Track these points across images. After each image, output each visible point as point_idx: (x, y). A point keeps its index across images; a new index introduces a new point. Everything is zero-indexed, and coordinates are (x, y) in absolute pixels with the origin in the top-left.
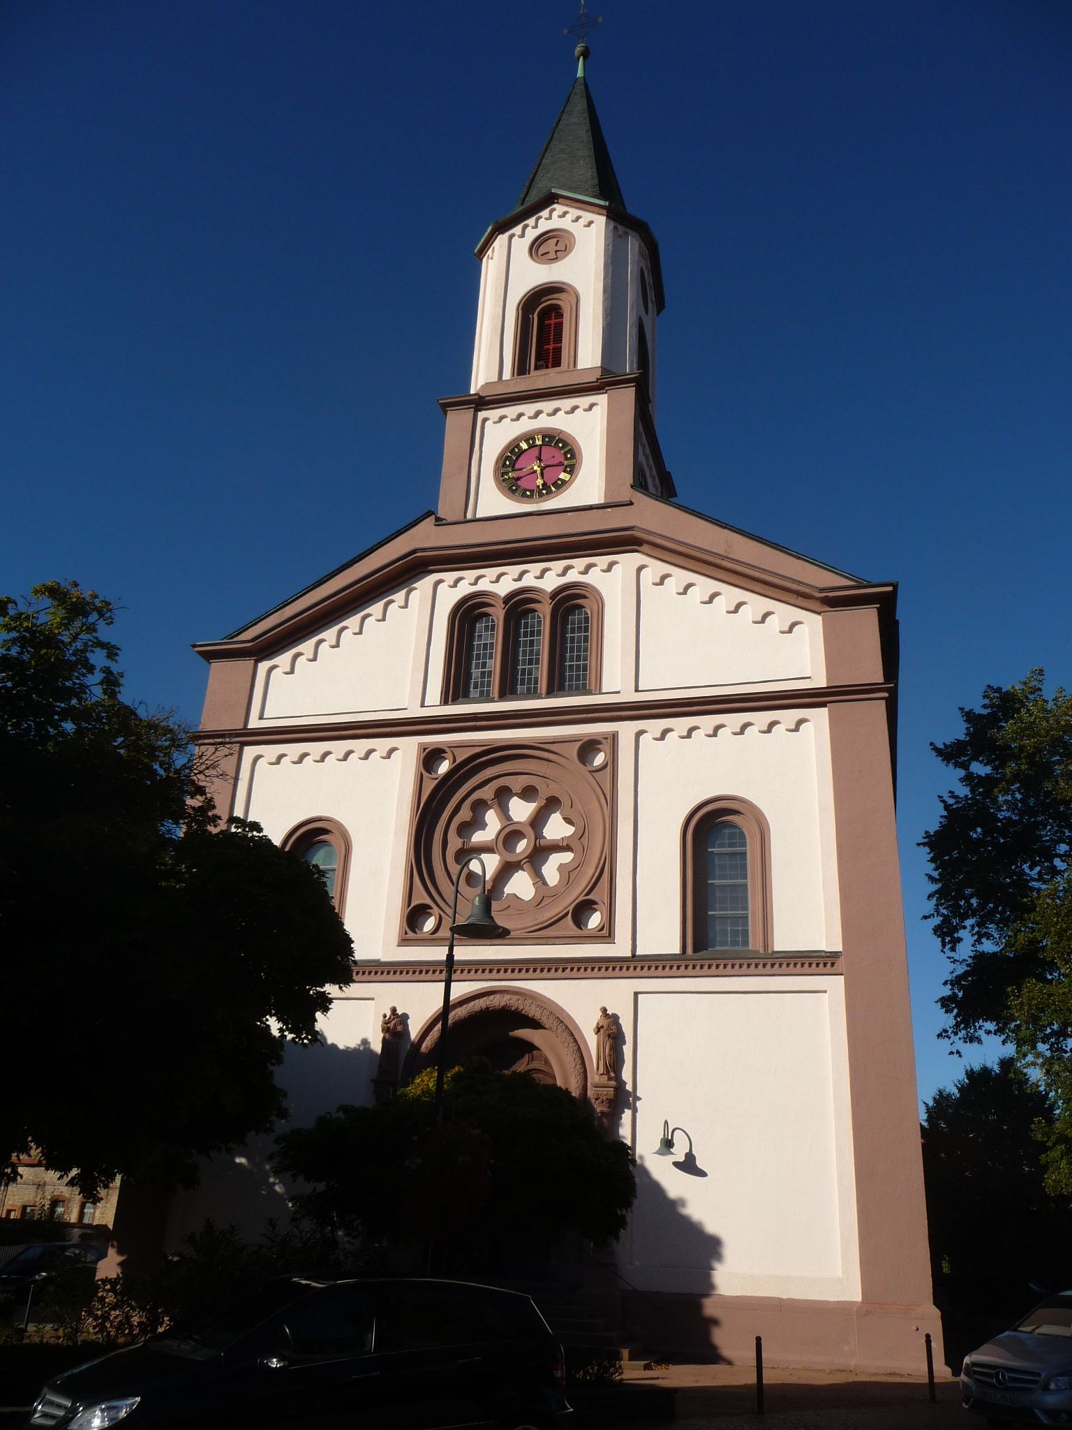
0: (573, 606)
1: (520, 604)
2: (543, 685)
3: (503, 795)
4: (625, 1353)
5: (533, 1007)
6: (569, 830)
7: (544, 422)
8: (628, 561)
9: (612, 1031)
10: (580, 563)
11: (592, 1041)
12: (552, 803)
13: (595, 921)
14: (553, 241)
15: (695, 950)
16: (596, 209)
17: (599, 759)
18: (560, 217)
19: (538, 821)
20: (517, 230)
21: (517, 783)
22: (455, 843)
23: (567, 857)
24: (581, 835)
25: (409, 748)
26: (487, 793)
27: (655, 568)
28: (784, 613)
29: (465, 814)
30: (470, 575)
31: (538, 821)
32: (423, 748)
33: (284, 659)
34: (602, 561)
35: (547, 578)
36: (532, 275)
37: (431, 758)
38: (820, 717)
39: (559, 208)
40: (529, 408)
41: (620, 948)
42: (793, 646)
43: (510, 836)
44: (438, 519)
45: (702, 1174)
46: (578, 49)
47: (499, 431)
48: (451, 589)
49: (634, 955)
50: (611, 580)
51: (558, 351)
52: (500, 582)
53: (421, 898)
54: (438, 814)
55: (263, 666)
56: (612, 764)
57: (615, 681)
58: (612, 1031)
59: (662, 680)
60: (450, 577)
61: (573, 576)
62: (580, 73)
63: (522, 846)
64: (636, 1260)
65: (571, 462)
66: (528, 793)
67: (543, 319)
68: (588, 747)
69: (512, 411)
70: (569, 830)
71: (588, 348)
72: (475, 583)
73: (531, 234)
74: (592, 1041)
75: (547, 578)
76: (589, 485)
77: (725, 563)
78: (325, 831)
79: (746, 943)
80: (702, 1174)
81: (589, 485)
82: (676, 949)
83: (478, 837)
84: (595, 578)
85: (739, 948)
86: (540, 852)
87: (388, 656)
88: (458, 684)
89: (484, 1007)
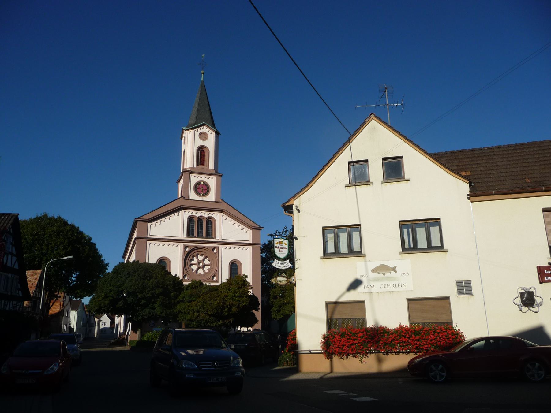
0: (210, 221)
1: (200, 219)
2: (204, 235)
3: (198, 254)
4: (75, 331)
6: (209, 263)
7: (203, 179)
10: (212, 213)
12: (206, 257)
13: (215, 279)
17: (215, 251)
19: (204, 260)
20: (196, 129)
22: (189, 264)
23: (209, 267)
24: (211, 264)
25: (181, 245)
26: (195, 254)
27: (225, 216)
28: (246, 229)
29: (191, 258)
30: (191, 211)
31: (204, 260)
33: (154, 223)
34: (216, 213)
35: (206, 215)
36: (200, 143)
37: (186, 247)
38: (250, 248)
40: (201, 176)
42: (247, 235)
43: (199, 262)
46: (202, 72)
47: (195, 179)
48: (187, 213)
50: (218, 217)
51: (204, 161)
52: (197, 214)
53: (185, 273)
54: (187, 258)
55: (149, 224)
56: (218, 252)
57: (218, 237)
59: (227, 237)
60: (187, 211)
61: (210, 215)
62: (202, 80)
63: (201, 265)
66: (202, 255)
67: (201, 153)
68: (214, 248)
69: (197, 175)
70: (209, 263)
73: (199, 132)
75: (206, 215)
76: (212, 197)
81: (212, 197)
83: (193, 262)
84: (214, 216)
86: (204, 265)
87: (175, 225)
88: (190, 233)
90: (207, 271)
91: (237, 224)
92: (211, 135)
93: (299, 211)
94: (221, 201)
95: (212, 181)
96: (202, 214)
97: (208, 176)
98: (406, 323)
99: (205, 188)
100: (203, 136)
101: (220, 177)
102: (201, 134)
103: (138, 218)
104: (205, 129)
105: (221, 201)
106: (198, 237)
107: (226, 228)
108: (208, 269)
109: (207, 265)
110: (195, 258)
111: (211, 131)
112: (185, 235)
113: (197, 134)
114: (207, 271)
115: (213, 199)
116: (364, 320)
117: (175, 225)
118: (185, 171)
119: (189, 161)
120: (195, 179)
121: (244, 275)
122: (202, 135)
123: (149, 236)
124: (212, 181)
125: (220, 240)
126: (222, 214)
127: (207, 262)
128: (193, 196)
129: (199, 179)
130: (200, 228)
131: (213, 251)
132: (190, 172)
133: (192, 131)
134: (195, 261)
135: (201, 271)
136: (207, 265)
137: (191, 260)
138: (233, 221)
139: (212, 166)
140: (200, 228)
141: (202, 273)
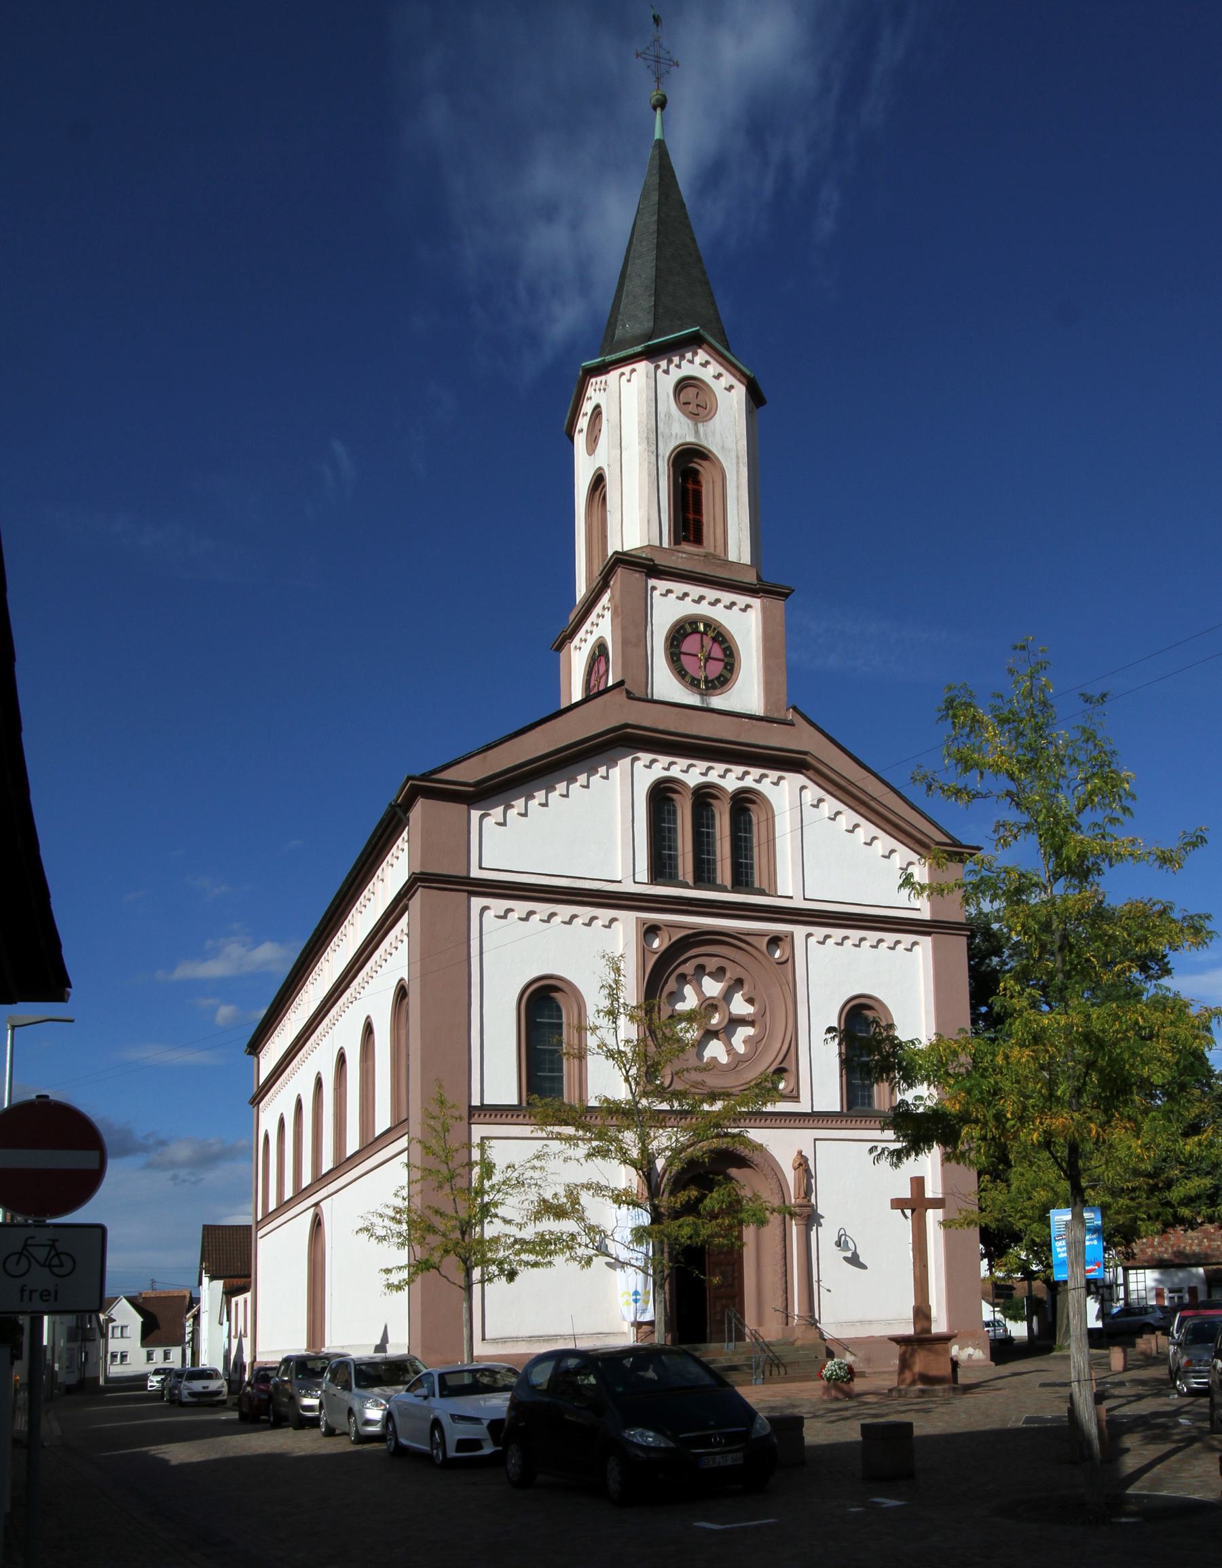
0: (744, 804)
1: (704, 796)
5: (737, 1145)
7: (704, 609)
8: (794, 780)
9: (803, 1165)
10: (756, 772)
11: (790, 1175)
12: (739, 983)
14: (694, 391)
15: (848, 1109)
16: (738, 375)
18: (701, 364)
19: (727, 996)
21: (712, 964)
23: (750, 1031)
25: (627, 923)
26: (688, 968)
27: (813, 792)
30: (664, 760)
32: (643, 922)
34: (774, 775)
36: (680, 431)
37: (651, 930)
38: (926, 942)
39: (702, 356)
41: (803, 1107)
44: (628, 692)
45: (864, 1267)
48: (648, 770)
49: (482, 1105)
50: (784, 793)
52: (692, 773)
56: (788, 961)
58: (803, 1165)
60: (646, 757)
61: (749, 782)
64: (513, 1413)
65: (687, 626)
66: (719, 974)
67: (688, 473)
68: (775, 941)
69: (680, 587)
71: (735, 535)
72: (667, 769)
73: (676, 374)
74: (790, 1175)
75: (731, 779)
76: (748, 693)
77: (873, 804)
78: (556, 989)
79: (870, 1104)
80: (864, 1267)
81: (748, 693)
82: (837, 1108)
84: (765, 787)
85: (866, 1108)
87: (594, 825)
89: (724, 1146)
90: (741, 1049)
91: (867, 829)
92: (731, 400)
94: (790, 715)
95: (745, 622)
96: (713, 777)
97: (727, 597)
99: (717, 652)
100: (691, 394)
101: (779, 605)
102: (684, 384)
103: (425, 777)
104: (700, 365)
105: (790, 715)
106: (696, 887)
107: (822, 847)
108: (683, 999)
110: (688, 990)
111: (728, 379)
112: (643, 874)
113: (668, 383)
114: (741, 1049)
116: (946, 1158)
117: (594, 825)
118: (623, 560)
119: (636, 521)
120: (669, 605)
122: (689, 393)
123: (475, 873)
124: (745, 622)
125: (798, 903)
126: (799, 779)
128: (666, 685)
129: (688, 608)
130: (703, 842)
132: (645, 566)
133: (643, 367)
135: (716, 1050)
138: (849, 817)
139: (738, 546)
140: (703, 842)
141: (724, 1059)
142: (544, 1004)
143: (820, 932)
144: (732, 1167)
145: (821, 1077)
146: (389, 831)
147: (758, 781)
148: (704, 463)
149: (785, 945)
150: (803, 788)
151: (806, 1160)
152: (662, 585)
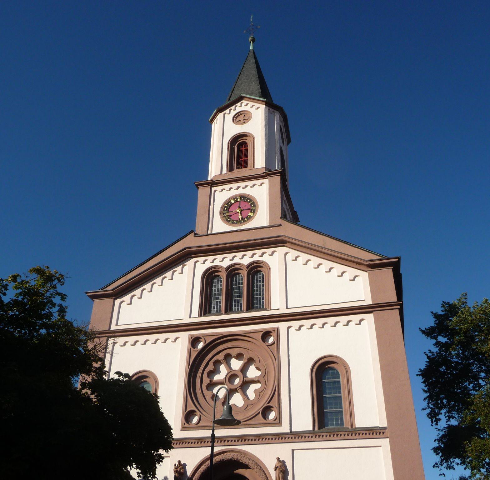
0: (256, 271)
1: (233, 271)
6: (259, 373)
7: (241, 191)
10: (259, 252)
12: (250, 361)
13: (272, 415)
17: (271, 340)
19: (244, 369)
20: (227, 111)
21: (234, 352)
23: (258, 386)
24: (264, 375)
25: (185, 337)
26: (220, 357)
27: (293, 253)
28: (351, 272)
29: (211, 367)
30: (210, 258)
31: (244, 369)
33: (127, 298)
34: (269, 251)
35: (245, 259)
38: (370, 318)
39: (245, 102)
41: (284, 429)
42: (356, 286)
43: (232, 377)
44: (196, 234)
48: (202, 265)
50: (273, 259)
52: (224, 261)
53: (191, 407)
54: (199, 366)
55: (118, 301)
57: (277, 304)
63: (237, 381)
66: (239, 356)
68: (266, 335)
71: (259, 159)
73: (233, 113)
75: (245, 259)
76: (262, 218)
78: (146, 377)
79: (342, 424)
81: (262, 218)
82: (310, 428)
83: (217, 378)
84: (266, 258)
85: (339, 427)
86: (246, 384)
87: (174, 296)
93: (272, 254)
98: (215, 436)
108: (219, 372)
109: (253, 381)
115: (265, 223)
121: (76, 387)
127: (253, 372)
130: (237, 291)
131: (489, 326)
134: (223, 373)
136: (253, 381)
137: (211, 374)
142: (327, 376)
143: (295, 324)
144: (187, 476)
145: (299, 408)
146: (278, 319)
147: (262, 256)
148: (247, 138)
149: (274, 334)
150: (286, 254)
151: (283, 463)
152: (219, 188)
